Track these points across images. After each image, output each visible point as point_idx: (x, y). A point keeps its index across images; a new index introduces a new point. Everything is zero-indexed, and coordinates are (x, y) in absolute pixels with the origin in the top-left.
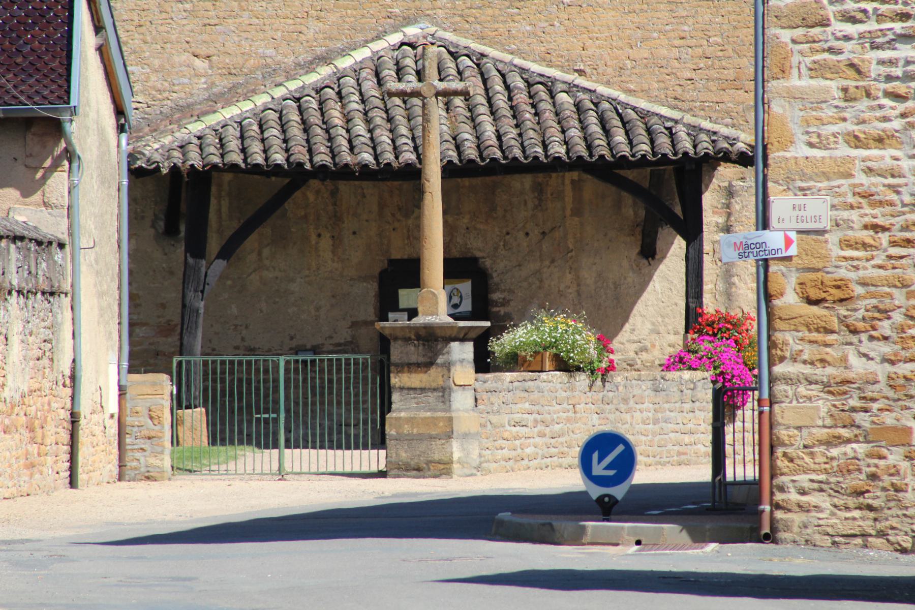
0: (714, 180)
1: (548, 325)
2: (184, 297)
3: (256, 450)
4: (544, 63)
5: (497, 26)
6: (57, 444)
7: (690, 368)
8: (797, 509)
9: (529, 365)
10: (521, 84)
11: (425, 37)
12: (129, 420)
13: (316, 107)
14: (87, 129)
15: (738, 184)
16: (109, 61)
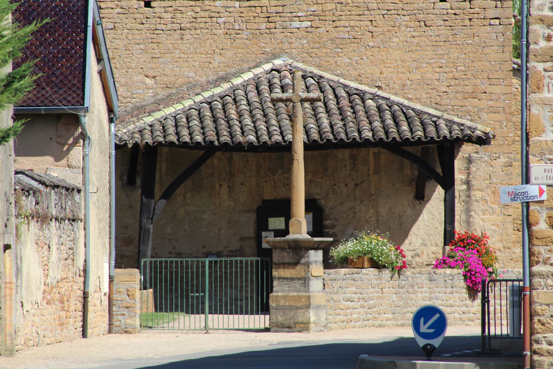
0: (460, 153)
1: (366, 240)
2: (140, 221)
3: (186, 315)
4: (357, 82)
5: (329, 59)
6: (76, 311)
7: (450, 267)
8: (547, 354)
9: (355, 264)
10: (344, 94)
11: (286, 66)
12: (115, 296)
13: (221, 108)
14: (93, 120)
15: (474, 155)
16: (105, 79)
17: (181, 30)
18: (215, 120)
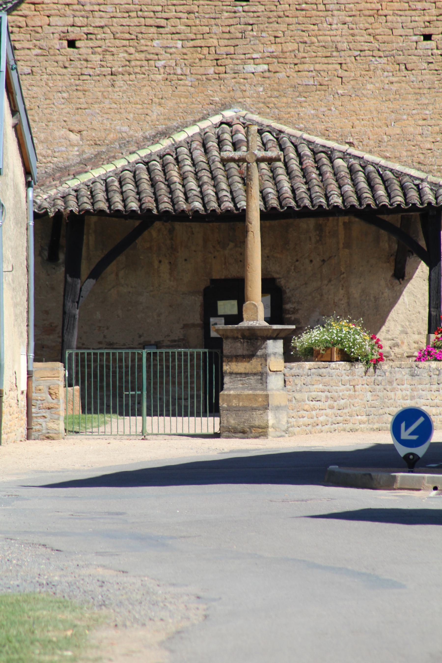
2: (64, 305)
3: (119, 417)
4: (324, 137)
5: (289, 110)
9: (322, 357)
10: (309, 153)
11: (238, 119)
12: (34, 395)
14: (7, 185)
17: (112, 74)
18: (153, 184)
